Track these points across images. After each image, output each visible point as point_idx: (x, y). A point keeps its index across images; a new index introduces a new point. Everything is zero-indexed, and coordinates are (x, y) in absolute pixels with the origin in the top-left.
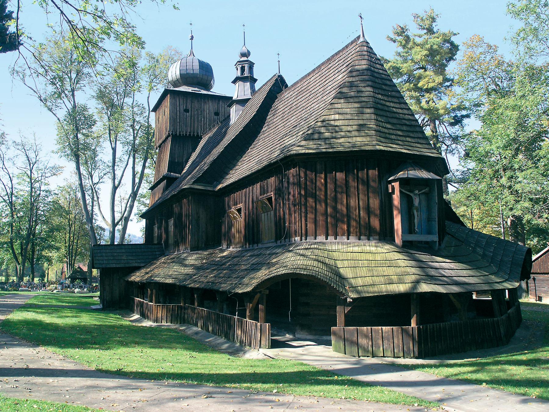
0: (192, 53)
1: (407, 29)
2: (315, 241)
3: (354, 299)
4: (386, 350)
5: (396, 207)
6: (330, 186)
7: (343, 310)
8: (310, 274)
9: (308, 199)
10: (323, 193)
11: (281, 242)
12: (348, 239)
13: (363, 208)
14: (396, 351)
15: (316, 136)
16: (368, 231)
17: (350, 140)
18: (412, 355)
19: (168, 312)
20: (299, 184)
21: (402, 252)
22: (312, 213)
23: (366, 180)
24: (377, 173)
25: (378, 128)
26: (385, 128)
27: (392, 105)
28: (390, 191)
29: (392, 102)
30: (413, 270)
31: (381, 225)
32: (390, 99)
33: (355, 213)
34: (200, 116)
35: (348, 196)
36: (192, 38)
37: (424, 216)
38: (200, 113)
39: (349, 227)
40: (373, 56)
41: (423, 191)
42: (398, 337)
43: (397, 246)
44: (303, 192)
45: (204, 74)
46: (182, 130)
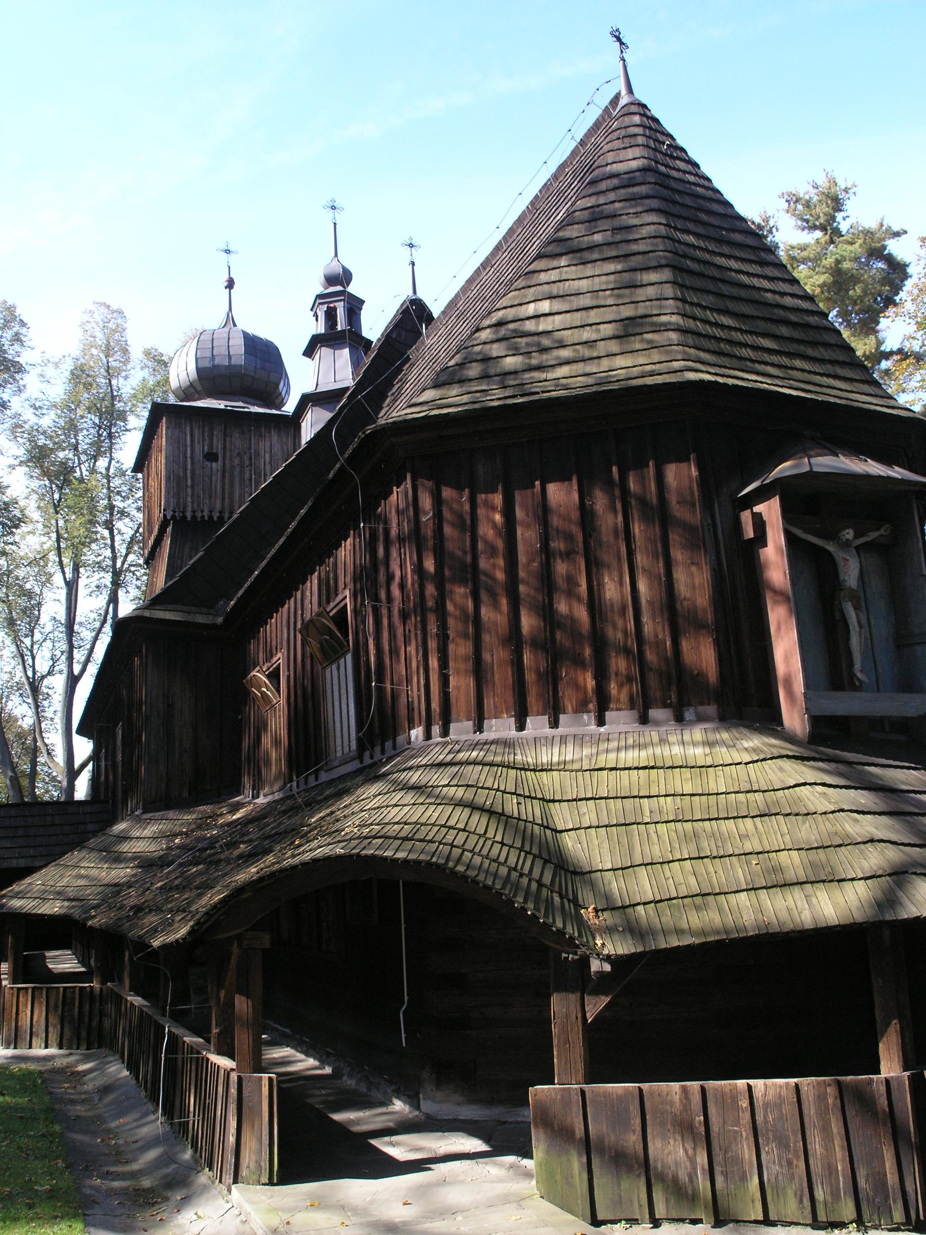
0: (230, 320)
1: (771, 228)
2: (478, 737)
3: (616, 961)
4: (776, 1188)
5: (775, 592)
6: (526, 536)
7: (575, 1011)
8: (422, 857)
9: (448, 586)
10: (501, 562)
11: (372, 757)
12: (601, 722)
13: (650, 603)
14: (819, 1194)
15: (474, 370)
16: (674, 688)
17: (591, 368)
18: (899, 1216)
19: (51, 1009)
20: (416, 537)
21: (814, 759)
22: (466, 636)
23: (655, 501)
24: (694, 472)
25: (690, 324)
26: (716, 325)
27: (733, 264)
28: (749, 533)
29: (736, 258)
30: (871, 826)
31: (722, 660)
32: (726, 250)
33: (620, 623)
34: (247, 470)
35: (593, 567)
36: (230, 284)
37: (883, 628)
38: (247, 463)
39: (601, 676)
40: (661, 138)
41: (872, 536)
42: (825, 1129)
43: (790, 739)
44: (430, 565)
45: (259, 366)
46: (199, 505)
